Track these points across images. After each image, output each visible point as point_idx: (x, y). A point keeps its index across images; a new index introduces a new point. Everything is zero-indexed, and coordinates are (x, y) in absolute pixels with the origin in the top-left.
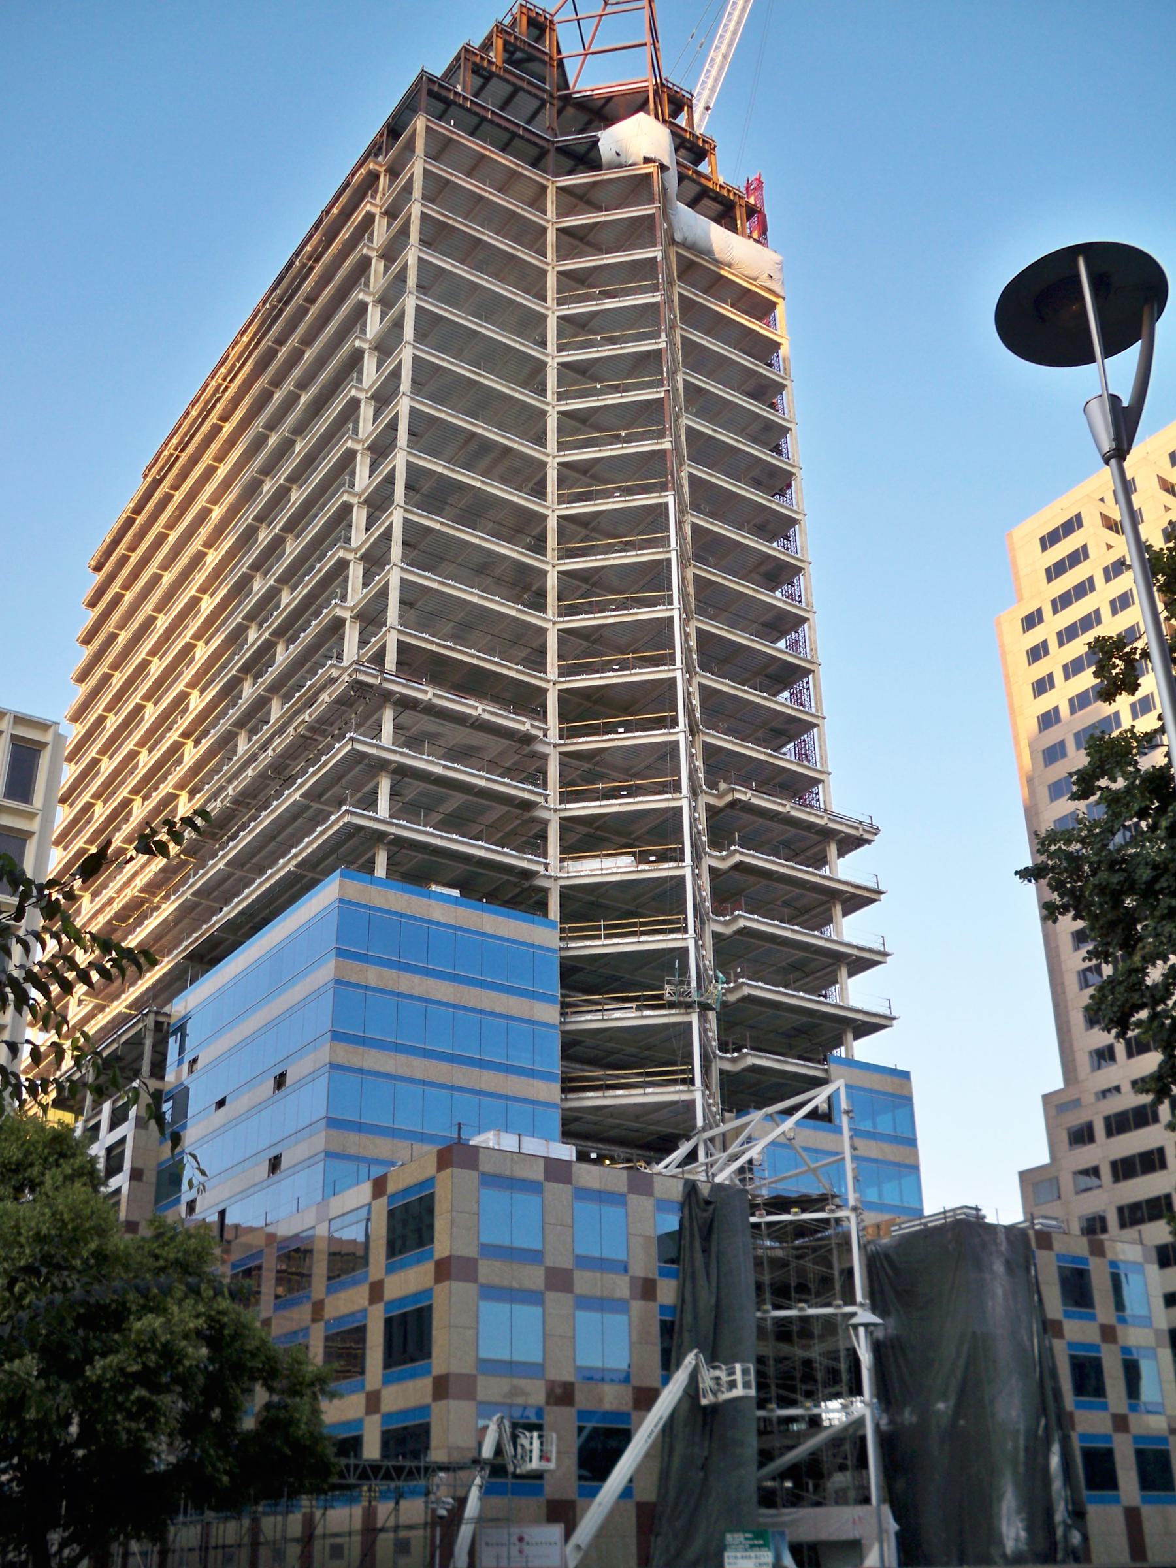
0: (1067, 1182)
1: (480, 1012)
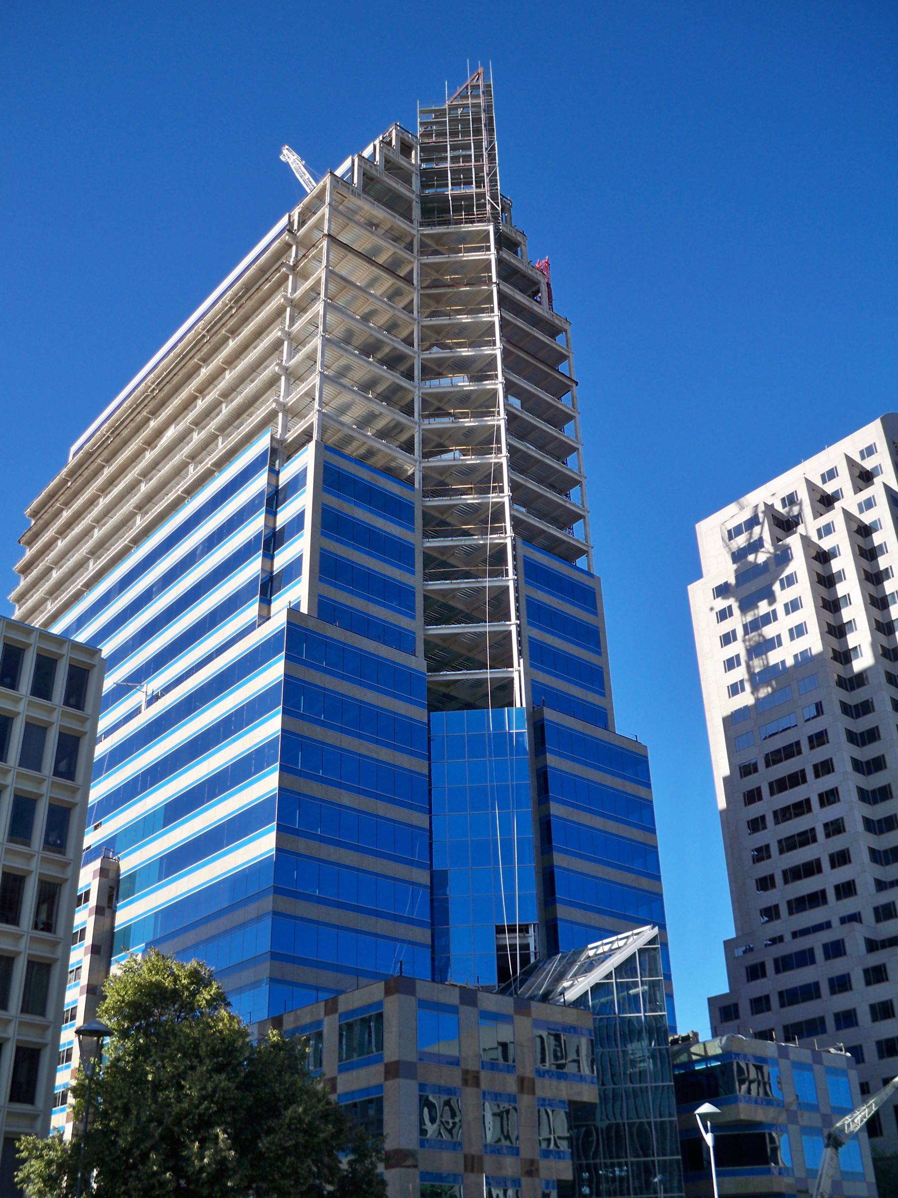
0: (745, 1008)
1: (376, 874)
